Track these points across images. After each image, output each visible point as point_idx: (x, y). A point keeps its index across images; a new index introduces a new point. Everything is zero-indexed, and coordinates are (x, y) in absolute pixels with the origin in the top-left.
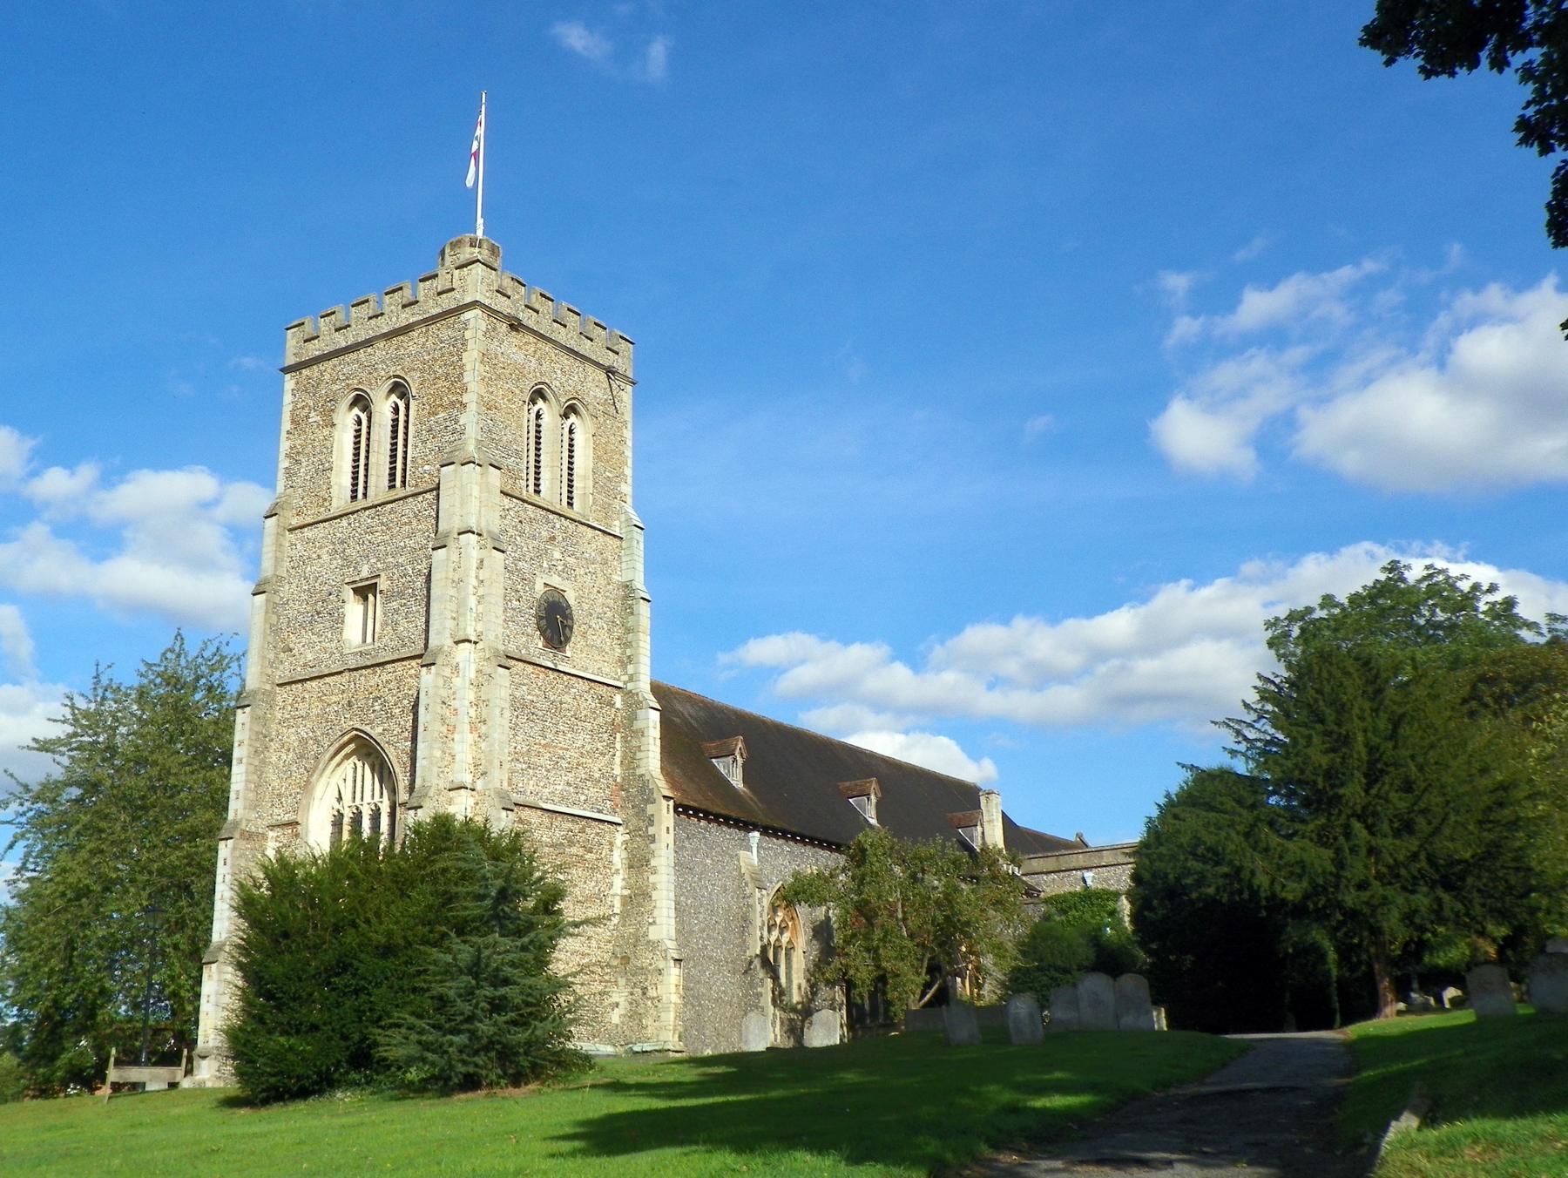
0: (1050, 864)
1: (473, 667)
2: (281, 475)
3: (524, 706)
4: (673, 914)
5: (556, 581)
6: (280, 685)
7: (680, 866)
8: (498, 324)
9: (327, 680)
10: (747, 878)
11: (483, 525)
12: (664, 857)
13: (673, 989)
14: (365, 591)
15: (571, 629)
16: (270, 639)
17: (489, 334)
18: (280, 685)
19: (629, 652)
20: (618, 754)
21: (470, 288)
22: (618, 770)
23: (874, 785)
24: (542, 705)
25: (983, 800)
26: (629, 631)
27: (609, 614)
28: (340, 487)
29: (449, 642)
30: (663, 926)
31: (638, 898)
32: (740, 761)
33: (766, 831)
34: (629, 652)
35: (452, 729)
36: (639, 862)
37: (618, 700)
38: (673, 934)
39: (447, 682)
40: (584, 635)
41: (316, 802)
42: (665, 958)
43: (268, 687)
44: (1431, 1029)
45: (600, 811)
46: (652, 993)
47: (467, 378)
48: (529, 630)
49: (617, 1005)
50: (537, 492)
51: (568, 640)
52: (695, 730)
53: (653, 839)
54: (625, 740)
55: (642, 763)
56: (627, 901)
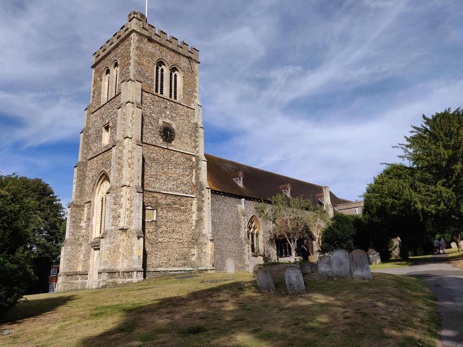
0: (345, 207)
1: (130, 146)
2: (91, 98)
3: (154, 160)
4: (210, 225)
5: (168, 121)
6: (89, 160)
7: (213, 210)
8: (143, 39)
9: (98, 156)
10: (240, 213)
11: (134, 100)
12: (207, 207)
13: (210, 249)
14: (107, 128)
15: (174, 136)
16: (85, 146)
17: (140, 41)
18: (89, 160)
19: (197, 144)
20: (194, 176)
21: (132, 27)
22: (194, 181)
23: (289, 186)
24: (162, 159)
25: (324, 189)
26: (197, 137)
27: (190, 132)
28: (104, 98)
29: (122, 138)
30: (207, 228)
31: (200, 220)
32: (242, 178)
33: (247, 198)
34: (197, 144)
35: (122, 167)
36: (200, 209)
37: (194, 159)
38: (211, 231)
39: (121, 152)
40: (180, 138)
41: (96, 195)
42: (207, 239)
43: (84, 161)
44: (264, 171)
45: (186, 193)
46: (204, 251)
47: (131, 55)
48: (157, 136)
49: (194, 255)
50: (162, 94)
51: (173, 140)
52: (217, 168)
53: (203, 202)
54: (196, 172)
55: (200, 178)
56: (197, 221)
